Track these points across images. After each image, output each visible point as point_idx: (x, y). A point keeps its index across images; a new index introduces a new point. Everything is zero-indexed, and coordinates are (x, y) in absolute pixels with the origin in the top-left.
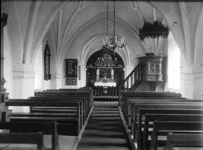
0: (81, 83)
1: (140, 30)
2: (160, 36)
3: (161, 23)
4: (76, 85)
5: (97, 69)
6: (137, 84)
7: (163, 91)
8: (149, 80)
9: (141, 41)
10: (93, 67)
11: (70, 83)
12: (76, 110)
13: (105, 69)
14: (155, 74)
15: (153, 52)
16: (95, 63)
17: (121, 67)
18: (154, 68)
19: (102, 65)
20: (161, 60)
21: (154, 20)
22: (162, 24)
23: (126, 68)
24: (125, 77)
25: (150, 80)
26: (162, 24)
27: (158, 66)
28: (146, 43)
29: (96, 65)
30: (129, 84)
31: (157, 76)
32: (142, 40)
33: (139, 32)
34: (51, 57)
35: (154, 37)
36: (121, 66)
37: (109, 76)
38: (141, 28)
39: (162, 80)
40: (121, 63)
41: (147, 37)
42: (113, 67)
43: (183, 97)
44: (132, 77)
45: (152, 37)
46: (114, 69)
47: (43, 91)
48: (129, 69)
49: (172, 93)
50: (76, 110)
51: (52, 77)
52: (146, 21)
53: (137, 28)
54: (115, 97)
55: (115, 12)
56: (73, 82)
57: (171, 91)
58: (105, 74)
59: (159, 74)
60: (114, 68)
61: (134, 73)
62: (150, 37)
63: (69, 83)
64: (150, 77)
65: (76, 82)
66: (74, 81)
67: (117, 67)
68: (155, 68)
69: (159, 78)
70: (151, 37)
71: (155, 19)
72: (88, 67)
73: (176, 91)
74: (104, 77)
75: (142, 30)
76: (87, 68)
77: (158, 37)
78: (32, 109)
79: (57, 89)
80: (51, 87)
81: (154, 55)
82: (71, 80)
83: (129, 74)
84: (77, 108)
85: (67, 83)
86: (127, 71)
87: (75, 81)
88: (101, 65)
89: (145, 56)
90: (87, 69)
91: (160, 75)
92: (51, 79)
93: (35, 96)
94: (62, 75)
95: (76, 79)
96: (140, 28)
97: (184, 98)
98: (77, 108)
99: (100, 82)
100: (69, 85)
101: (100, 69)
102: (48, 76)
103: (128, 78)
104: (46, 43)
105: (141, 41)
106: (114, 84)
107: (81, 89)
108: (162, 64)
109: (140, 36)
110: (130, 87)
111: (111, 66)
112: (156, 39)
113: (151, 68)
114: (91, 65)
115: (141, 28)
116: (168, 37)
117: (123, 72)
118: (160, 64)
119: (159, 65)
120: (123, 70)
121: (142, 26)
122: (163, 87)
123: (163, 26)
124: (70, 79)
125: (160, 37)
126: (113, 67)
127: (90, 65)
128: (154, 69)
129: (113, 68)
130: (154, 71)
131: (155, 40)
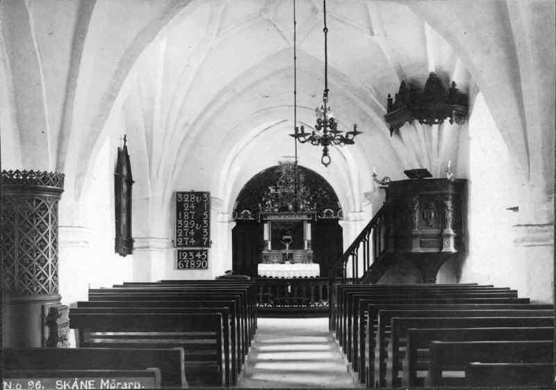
0: (220, 260)
1: (390, 100)
2: (445, 118)
3: (448, 80)
4: (207, 268)
6: (382, 263)
7: (458, 281)
8: (417, 249)
9: (391, 135)
10: (252, 217)
11: (189, 262)
12: (214, 341)
14: (434, 231)
15: (425, 166)
17: (334, 217)
18: (431, 214)
20: (451, 190)
21: (428, 70)
22: (451, 82)
23: (347, 219)
24: (346, 246)
25: (421, 250)
26: (451, 82)
27: (441, 209)
28: (404, 139)
29: (261, 212)
30: (356, 267)
31: (441, 238)
32: (393, 133)
33: (385, 107)
34: (134, 186)
35: (430, 123)
36: (332, 212)
37: (298, 244)
38: (393, 96)
39: (452, 249)
41: (411, 123)
43: (521, 296)
44: (368, 242)
45: (426, 123)
46: (311, 222)
47: (114, 286)
48: (353, 223)
49: (483, 288)
50: (214, 341)
51: (135, 245)
52: (405, 76)
53: (379, 96)
54: (317, 304)
55: (293, 93)
56: (196, 259)
57: (483, 282)
58: (288, 240)
59: (445, 231)
61: (372, 230)
62: (417, 122)
63: (185, 264)
64: (419, 239)
65: (206, 259)
66: (199, 255)
67: (322, 216)
68: (433, 215)
69: (445, 243)
70: (421, 122)
71: (432, 69)
72: (239, 218)
74: (285, 247)
75: (396, 103)
76: (237, 221)
77: (441, 122)
78: (83, 341)
79: (152, 281)
81: (431, 176)
82: (191, 254)
83: (357, 237)
84: (214, 333)
85: (182, 263)
86: (348, 226)
87: (203, 257)
89: (406, 178)
90: (234, 224)
91: (449, 236)
92: (134, 252)
93: (90, 299)
94: (165, 241)
95: (206, 251)
96: (389, 96)
97: (527, 300)
98: (214, 333)
100: (185, 267)
101: (273, 223)
102: (125, 244)
103: (355, 245)
104: (121, 143)
105: (391, 135)
106: (311, 270)
107: (220, 280)
108: (453, 202)
109: (388, 119)
110: (361, 274)
112: (435, 127)
113: (423, 215)
114: (248, 211)
115: (393, 96)
116: (468, 121)
117: (340, 229)
118: (449, 204)
119: (445, 206)
120: (339, 226)
121: (394, 89)
122: (457, 269)
123: (456, 87)
124: (187, 251)
125: (447, 121)
128: (430, 217)
130: (431, 223)
131: (431, 132)
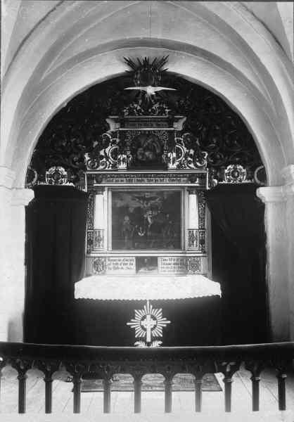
5: (94, 192)
13: (148, 195)
16: (82, 159)
19: (128, 169)
40: (239, 155)
42: (192, 178)
60: (203, 184)
73: (195, 415)
76: (36, 188)
80: (9, 339)
88: (123, 166)
90: (30, 195)
99: (150, 301)
101: (116, 194)
111: (184, 175)
114: (62, 169)
126: (192, 178)
127: (53, 169)
129: (196, 184)
